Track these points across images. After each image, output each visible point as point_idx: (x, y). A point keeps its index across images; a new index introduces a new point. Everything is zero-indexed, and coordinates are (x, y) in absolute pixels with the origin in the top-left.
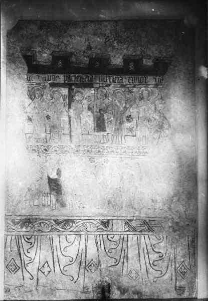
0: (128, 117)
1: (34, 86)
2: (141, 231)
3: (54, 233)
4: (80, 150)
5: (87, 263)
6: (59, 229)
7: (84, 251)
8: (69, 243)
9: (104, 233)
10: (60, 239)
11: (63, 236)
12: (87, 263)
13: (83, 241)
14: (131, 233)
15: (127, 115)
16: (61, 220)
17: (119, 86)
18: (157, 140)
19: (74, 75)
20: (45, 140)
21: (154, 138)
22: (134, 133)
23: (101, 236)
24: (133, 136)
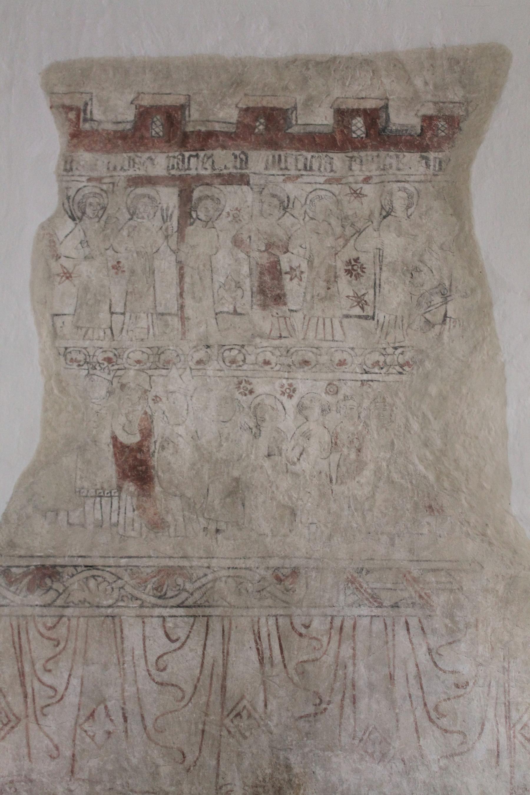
0: (349, 263)
1: (81, 185)
2: (395, 606)
3: (127, 611)
4: (252, 787)
5: (230, 705)
6: (144, 597)
7: (219, 670)
8: (173, 641)
9: (281, 612)
10: (148, 629)
11: (155, 620)
12: (230, 705)
13: (215, 638)
14: (365, 611)
15: (346, 258)
16: (149, 570)
17: (322, 180)
18: (438, 328)
19: (194, 153)
20: (108, 332)
21: (427, 321)
22: (369, 311)
23: (272, 621)
24: (366, 318)
